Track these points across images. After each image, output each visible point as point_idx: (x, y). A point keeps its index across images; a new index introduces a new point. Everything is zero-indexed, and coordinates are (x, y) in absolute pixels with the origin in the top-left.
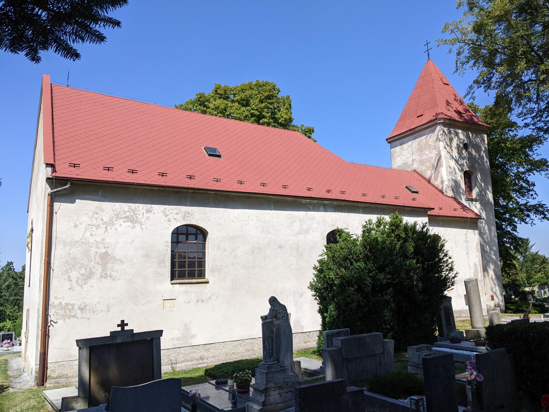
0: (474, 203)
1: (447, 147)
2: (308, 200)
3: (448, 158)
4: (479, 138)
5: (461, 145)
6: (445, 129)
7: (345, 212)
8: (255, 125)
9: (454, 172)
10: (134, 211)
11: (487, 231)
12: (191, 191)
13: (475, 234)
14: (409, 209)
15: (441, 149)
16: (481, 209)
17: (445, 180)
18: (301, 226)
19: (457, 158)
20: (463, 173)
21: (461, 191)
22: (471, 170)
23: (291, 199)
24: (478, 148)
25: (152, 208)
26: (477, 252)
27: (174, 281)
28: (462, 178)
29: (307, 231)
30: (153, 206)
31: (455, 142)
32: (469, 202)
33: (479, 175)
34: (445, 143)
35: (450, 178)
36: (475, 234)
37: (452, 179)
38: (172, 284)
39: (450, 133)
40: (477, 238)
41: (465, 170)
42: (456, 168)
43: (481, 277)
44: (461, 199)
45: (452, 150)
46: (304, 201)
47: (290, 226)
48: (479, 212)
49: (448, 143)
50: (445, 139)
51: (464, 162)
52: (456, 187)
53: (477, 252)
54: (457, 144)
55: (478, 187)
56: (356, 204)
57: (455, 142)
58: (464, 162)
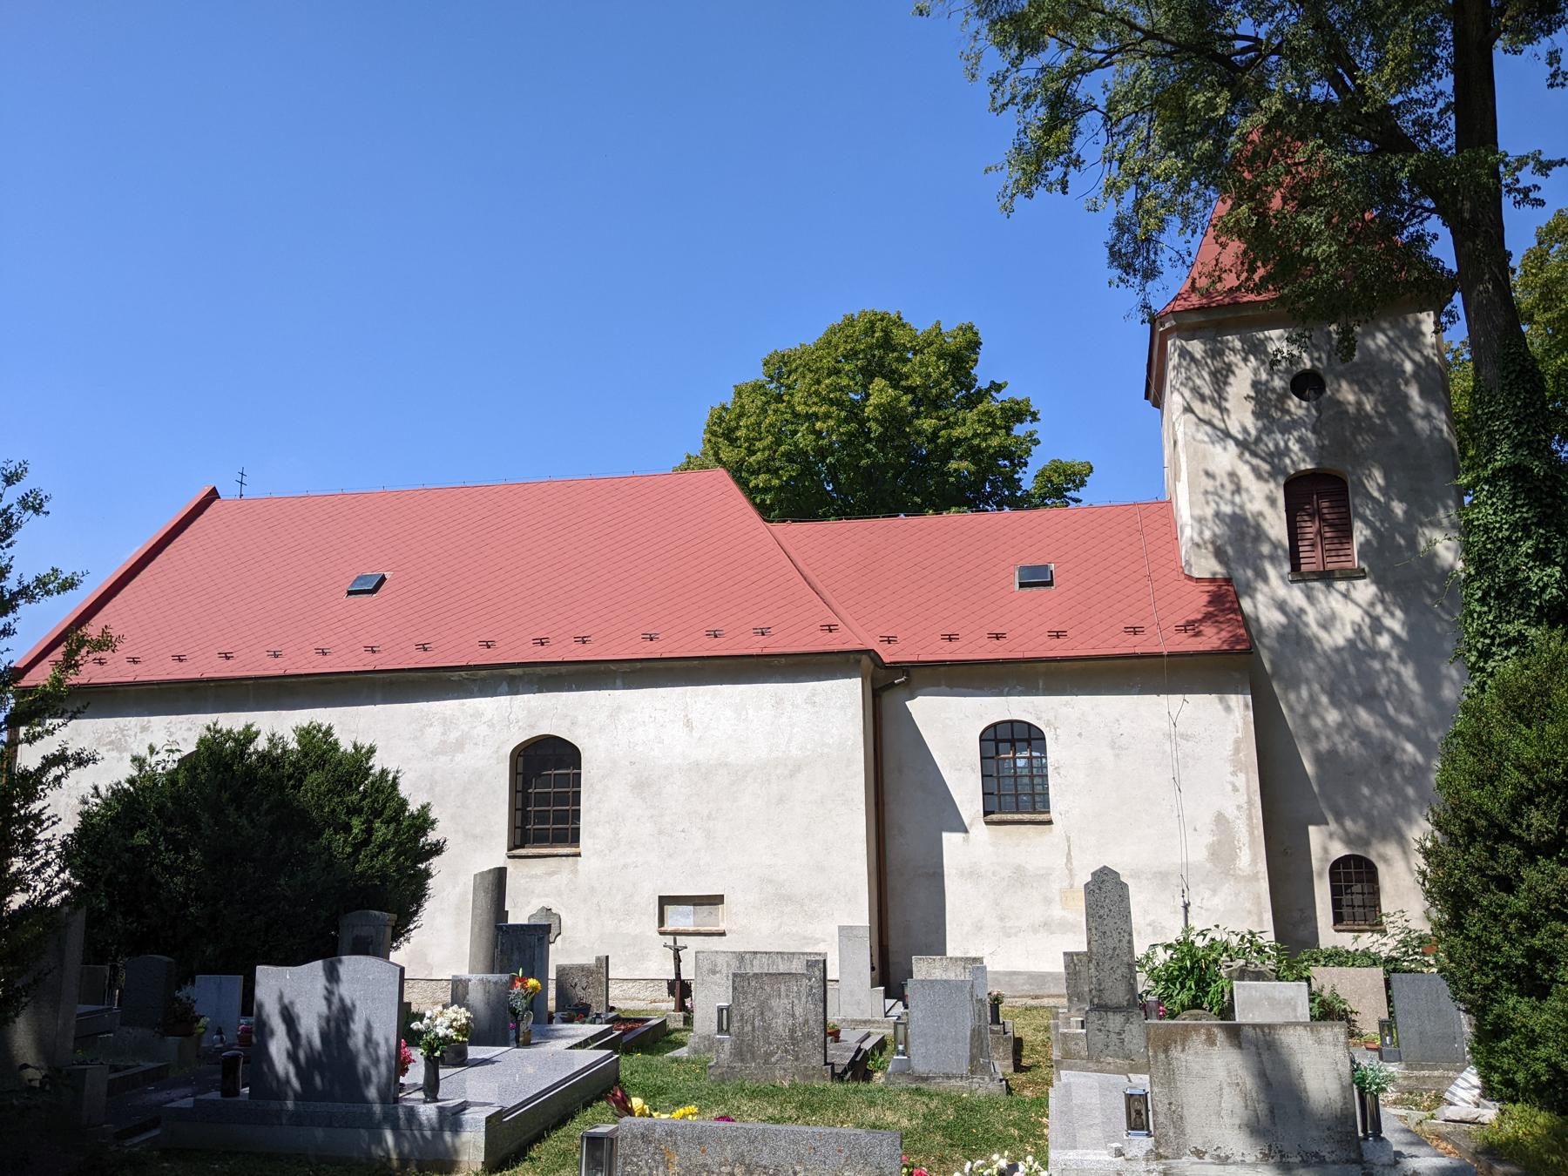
0: (1341, 586)
1: (1197, 406)
2: (462, 673)
3: (1204, 442)
4: (1384, 332)
5: (1278, 383)
6: (1196, 347)
7: (570, 689)
8: (983, 350)
9: (1229, 487)
10: (122, 730)
11: (1414, 685)
12: (212, 684)
13: (1228, 709)
15: (1174, 418)
16: (1383, 601)
17: (1261, 514)
18: (444, 734)
19: (1253, 432)
20: (1282, 481)
21: (1265, 549)
22: (1329, 464)
23: (420, 674)
24: (1373, 374)
25: (149, 722)
26: (1234, 773)
27: (994, 817)
28: (1272, 501)
29: (460, 745)
30: (152, 718)
32: (1310, 584)
34: (1187, 394)
35: (1209, 512)
36: (1228, 709)
37: (1217, 514)
38: (1337, 931)
39: (1216, 353)
40: (1240, 724)
41: (1292, 472)
42: (1244, 472)
43: (1254, 862)
44: (1265, 579)
45: (1223, 410)
46: (455, 676)
47: (416, 738)
50: (1189, 378)
53: (1234, 773)
56: (602, 667)
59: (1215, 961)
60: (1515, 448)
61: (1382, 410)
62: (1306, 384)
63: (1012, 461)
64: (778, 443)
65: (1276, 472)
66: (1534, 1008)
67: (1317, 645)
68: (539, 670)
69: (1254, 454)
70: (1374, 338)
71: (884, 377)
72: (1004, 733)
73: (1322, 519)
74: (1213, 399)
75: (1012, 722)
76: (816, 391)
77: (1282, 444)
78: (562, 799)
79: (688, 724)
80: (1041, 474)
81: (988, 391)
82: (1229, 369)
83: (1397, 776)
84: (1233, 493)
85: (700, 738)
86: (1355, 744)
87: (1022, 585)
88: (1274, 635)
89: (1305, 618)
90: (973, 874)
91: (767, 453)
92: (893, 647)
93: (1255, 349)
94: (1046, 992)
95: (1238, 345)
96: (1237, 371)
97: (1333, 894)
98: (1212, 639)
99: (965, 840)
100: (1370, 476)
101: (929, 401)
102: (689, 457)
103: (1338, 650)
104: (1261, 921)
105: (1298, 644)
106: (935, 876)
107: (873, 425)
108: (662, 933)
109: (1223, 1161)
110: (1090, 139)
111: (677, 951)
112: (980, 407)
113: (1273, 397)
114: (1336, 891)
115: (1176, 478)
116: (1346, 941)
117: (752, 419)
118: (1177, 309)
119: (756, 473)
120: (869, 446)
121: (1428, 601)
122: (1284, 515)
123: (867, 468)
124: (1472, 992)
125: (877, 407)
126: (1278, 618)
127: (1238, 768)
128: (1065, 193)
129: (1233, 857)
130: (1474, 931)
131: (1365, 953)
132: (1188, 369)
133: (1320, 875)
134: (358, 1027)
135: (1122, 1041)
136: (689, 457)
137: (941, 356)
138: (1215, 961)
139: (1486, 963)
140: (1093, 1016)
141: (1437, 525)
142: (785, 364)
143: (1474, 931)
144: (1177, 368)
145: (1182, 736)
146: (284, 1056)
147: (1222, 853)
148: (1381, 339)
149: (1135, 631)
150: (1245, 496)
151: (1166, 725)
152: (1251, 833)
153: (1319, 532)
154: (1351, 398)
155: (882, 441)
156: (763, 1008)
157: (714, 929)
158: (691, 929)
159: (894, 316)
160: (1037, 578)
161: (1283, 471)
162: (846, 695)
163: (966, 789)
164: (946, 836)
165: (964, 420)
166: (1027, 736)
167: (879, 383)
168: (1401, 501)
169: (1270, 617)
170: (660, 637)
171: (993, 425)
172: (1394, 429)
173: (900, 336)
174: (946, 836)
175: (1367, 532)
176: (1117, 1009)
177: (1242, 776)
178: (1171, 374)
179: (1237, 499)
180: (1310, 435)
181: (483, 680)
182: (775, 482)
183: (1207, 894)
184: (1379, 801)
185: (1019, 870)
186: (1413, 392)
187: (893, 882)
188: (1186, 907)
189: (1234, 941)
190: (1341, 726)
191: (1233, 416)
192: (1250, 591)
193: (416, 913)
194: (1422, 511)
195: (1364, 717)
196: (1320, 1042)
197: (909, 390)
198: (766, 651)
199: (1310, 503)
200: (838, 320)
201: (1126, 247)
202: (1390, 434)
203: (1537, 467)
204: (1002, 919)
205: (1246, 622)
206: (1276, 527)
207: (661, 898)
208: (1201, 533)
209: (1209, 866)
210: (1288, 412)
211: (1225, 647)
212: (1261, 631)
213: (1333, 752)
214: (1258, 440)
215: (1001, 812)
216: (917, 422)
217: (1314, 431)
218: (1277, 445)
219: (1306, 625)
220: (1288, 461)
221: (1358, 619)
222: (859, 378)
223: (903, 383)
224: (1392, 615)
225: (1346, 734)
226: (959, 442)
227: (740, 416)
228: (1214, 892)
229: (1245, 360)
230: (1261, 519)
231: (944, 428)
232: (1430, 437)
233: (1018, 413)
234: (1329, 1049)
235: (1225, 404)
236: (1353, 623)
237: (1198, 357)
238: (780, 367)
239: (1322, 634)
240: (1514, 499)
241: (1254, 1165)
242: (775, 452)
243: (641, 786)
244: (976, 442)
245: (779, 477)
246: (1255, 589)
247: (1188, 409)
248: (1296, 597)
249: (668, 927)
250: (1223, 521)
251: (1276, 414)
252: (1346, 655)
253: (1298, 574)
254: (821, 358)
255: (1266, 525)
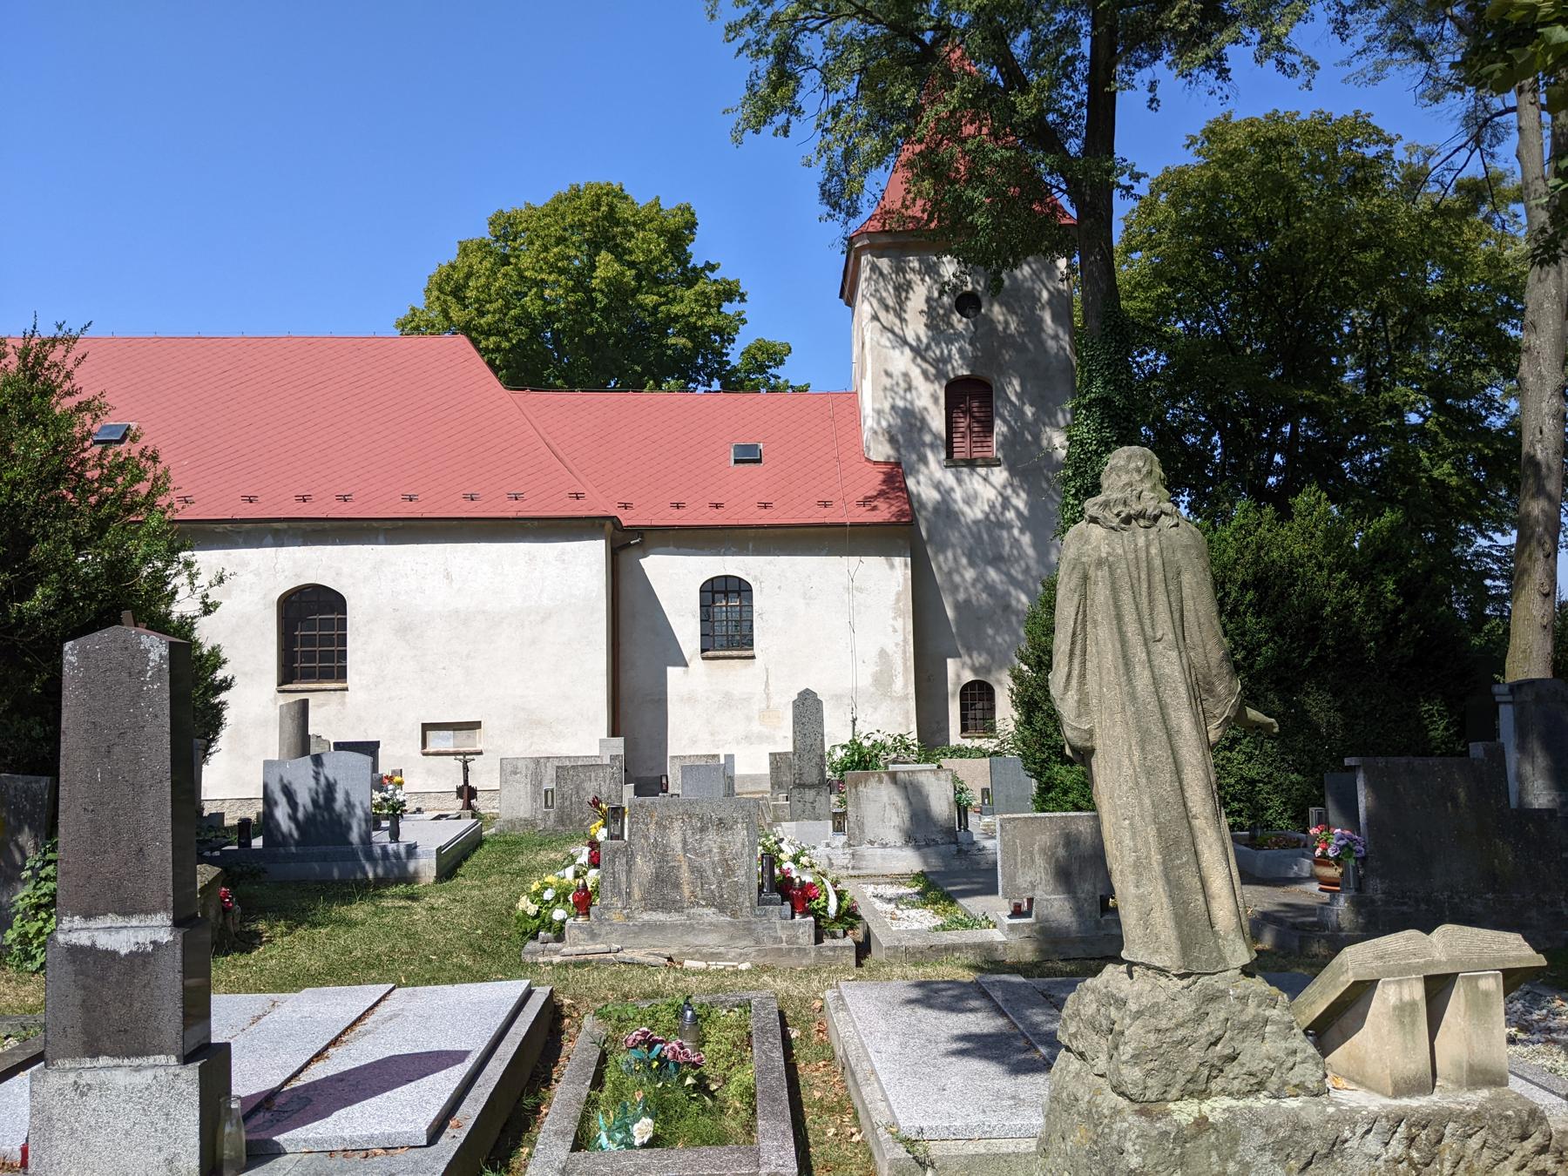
0: (982, 471)
1: (882, 314)
6: (884, 264)
7: (334, 543)
8: (699, 230)
9: (903, 385)
11: (1030, 551)
14: (536, 523)
16: (1012, 485)
19: (925, 340)
20: (944, 383)
21: (928, 438)
22: (983, 373)
24: (1020, 301)
27: (709, 654)
28: (936, 400)
31: (917, 299)
33: (1016, 383)
35: (887, 406)
36: (892, 566)
37: (893, 407)
39: (899, 269)
40: (901, 580)
41: (952, 376)
42: (916, 373)
43: (906, 686)
45: (902, 320)
46: (220, 528)
48: (1001, 494)
49: (890, 302)
50: (877, 290)
51: (954, 351)
52: (907, 429)
54: (928, 300)
55: (1005, 421)
56: (365, 524)
57: (917, 299)
58: (954, 351)
59: (876, 756)
60: (1106, 383)
61: (1023, 330)
62: (967, 303)
63: (721, 337)
64: (507, 306)
65: (940, 374)
66: (1068, 772)
67: (962, 519)
68: (303, 524)
69: (924, 359)
70: (1021, 269)
71: (609, 250)
72: (720, 586)
73: (972, 417)
74: (895, 310)
75: (726, 577)
76: (545, 258)
77: (946, 352)
78: (328, 640)
79: (448, 576)
80: (748, 351)
81: (703, 269)
82: (909, 286)
83: (1014, 619)
84: (905, 391)
85: (459, 589)
86: (984, 596)
87: (736, 462)
88: (930, 509)
89: (953, 494)
90: (690, 699)
91: (497, 316)
92: (630, 512)
93: (931, 270)
94: (746, 790)
95: (916, 265)
96: (915, 287)
97: (962, 710)
98: (884, 513)
99: (685, 672)
100: (1010, 383)
101: (648, 276)
102: (413, 309)
103: (976, 522)
104: (908, 727)
105: (948, 517)
106: (660, 701)
107: (599, 296)
108: (424, 754)
109: (884, 846)
110: (811, 96)
111: (465, 762)
112: (696, 288)
113: (941, 312)
114: (963, 707)
115: (863, 376)
116: (968, 743)
117: (483, 280)
118: (871, 229)
119: (488, 334)
120: (594, 315)
121: (1045, 485)
122: (944, 412)
123: (592, 337)
124: (1035, 763)
125: (603, 280)
126: (936, 496)
127: (898, 613)
128: (786, 136)
129: (891, 683)
130: (1038, 726)
131: (978, 749)
132: (877, 282)
133: (954, 695)
134: (340, 797)
135: (814, 808)
136: (413, 309)
137: (661, 232)
138: (876, 756)
139: (1043, 745)
140: (795, 792)
141: (1057, 426)
142: (511, 225)
143: (1038, 726)
144: (868, 280)
145: (857, 589)
146: (286, 818)
147: (882, 680)
148: (1026, 270)
149: (825, 504)
150: (914, 392)
151: (845, 580)
152: (905, 664)
153: (969, 426)
154: (1001, 318)
155: (605, 311)
156: (578, 789)
157: (472, 749)
158: (452, 750)
159: (616, 186)
160: (748, 456)
161: (945, 375)
162: (592, 554)
163: (686, 628)
164: (670, 669)
165: (682, 297)
166: (736, 589)
167: (604, 256)
168: (1032, 405)
169: (929, 495)
170: (420, 498)
171: (709, 306)
172: (1030, 346)
173: (623, 210)
174: (670, 669)
175: (1005, 429)
176: (811, 786)
177: (900, 621)
178: (862, 285)
179: (908, 396)
180: (967, 346)
181: (248, 532)
182: (505, 345)
183: (870, 711)
184: (999, 640)
185: (728, 695)
186: (1047, 317)
187: (624, 707)
188: (854, 721)
189: (890, 742)
190: (975, 581)
191: (910, 327)
192: (913, 471)
193: (213, 740)
194: (1046, 414)
195: (992, 574)
196: (938, 779)
197: (632, 265)
198: (520, 515)
199: (964, 402)
200: (565, 189)
201: (834, 185)
202: (1028, 350)
203: (1118, 400)
204: (712, 734)
205: (909, 497)
206: (937, 422)
207: (424, 725)
208: (879, 423)
209: (872, 689)
210: (952, 326)
211: (894, 519)
212: (922, 505)
213: (968, 601)
214: (928, 347)
215: (714, 650)
216: (640, 297)
217: (971, 344)
218: (942, 352)
219: (955, 501)
220: (949, 367)
221: (993, 497)
222: (585, 247)
223: (627, 257)
224: (1018, 495)
225: (979, 586)
226: (676, 319)
227: (468, 276)
228: (875, 709)
229: (923, 280)
230: (925, 413)
231: (663, 304)
232: (1057, 354)
233: (730, 293)
234: (943, 783)
235: (904, 315)
236: (988, 500)
237: (885, 272)
238: (506, 228)
239: (966, 509)
240: (1102, 422)
241: (901, 847)
242: (505, 315)
243: (404, 630)
244: (693, 320)
245: (509, 340)
246: (918, 471)
247: (875, 318)
248: (949, 478)
249: (428, 749)
250: (896, 413)
251: (943, 326)
252: (981, 525)
253: (951, 461)
254: (548, 226)
255: (928, 418)
